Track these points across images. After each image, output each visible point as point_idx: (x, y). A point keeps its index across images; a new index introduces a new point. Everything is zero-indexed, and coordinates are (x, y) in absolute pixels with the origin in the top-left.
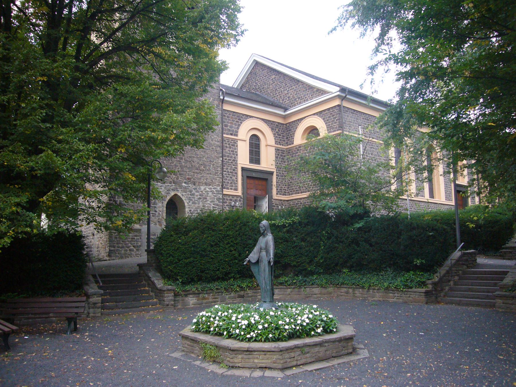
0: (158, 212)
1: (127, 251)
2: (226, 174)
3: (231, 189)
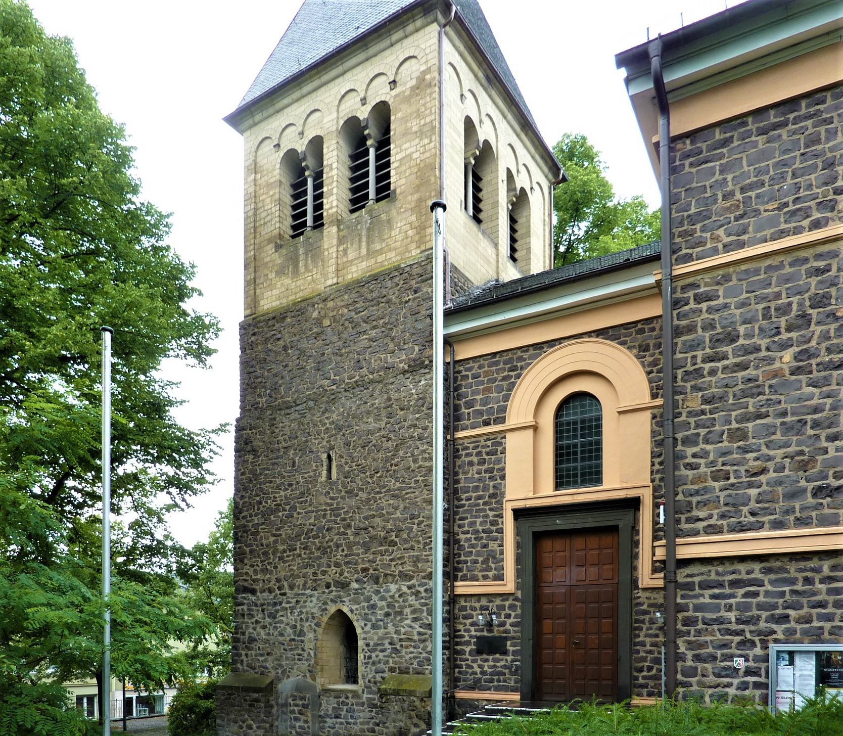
0: (308, 650)
2: (469, 540)
3: (485, 578)
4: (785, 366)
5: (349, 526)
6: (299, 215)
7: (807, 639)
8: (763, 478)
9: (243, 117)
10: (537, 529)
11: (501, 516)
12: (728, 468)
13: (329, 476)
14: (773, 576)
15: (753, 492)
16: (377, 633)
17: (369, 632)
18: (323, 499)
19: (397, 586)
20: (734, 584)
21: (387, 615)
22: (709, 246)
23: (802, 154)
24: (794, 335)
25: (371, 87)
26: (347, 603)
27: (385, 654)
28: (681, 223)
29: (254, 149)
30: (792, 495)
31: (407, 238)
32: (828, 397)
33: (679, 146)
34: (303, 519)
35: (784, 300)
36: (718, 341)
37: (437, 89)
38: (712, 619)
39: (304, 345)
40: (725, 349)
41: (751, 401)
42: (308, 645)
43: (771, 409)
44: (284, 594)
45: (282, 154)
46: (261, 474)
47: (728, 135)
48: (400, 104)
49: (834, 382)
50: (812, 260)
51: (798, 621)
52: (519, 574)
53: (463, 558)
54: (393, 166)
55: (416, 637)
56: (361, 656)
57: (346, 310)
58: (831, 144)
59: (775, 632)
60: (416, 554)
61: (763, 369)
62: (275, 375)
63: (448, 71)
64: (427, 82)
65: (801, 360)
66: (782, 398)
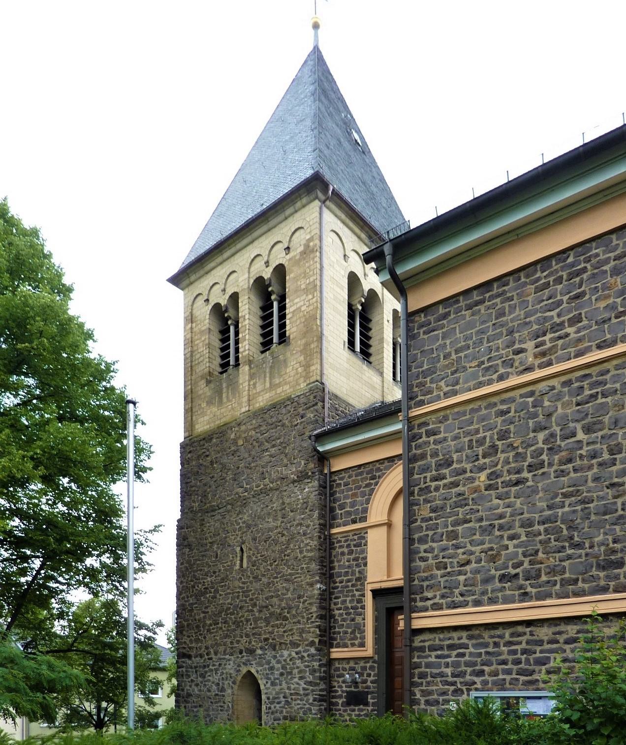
2: (341, 615)
3: (353, 645)
4: (481, 484)
5: (255, 605)
6: (225, 357)
7: (495, 688)
8: (468, 568)
9: (178, 280)
10: (388, 606)
11: (363, 595)
12: (446, 560)
13: (241, 566)
14: (474, 641)
15: (462, 578)
16: (274, 689)
17: (269, 688)
18: (237, 583)
19: (288, 652)
20: (451, 647)
21: (282, 674)
22: (435, 394)
23: (494, 324)
24: (487, 460)
25: (272, 252)
26: (254, 666)
27: (281, 705)
28: (418, 377)
29: (190, 303)
30: (487, 580)
31: (297, 374)
32: (509, 507)
33: (417, 319)
34: (224, 600)
35: (481, 435)
36: (440, 465)
37: (318, 254)
38: (436, 674)
39: (225, 460)
40: (444, 471)
41: (461, 510)
42: (228, 699)
43: (473, 516)
44: (211, 659)
45: (210, 307)
46: (194, 564)
47: (447, 310)
48: (293, 266)
49: (512, 495)
50: (499, 404)
51: (490, 675)
52: (376, 641)
53: (337, 630)
54: (288, 317)
55: (302, 692)
56: (264, 707)
57: (254, 433)
58: (512, 316)
59: (475, 683)
60: (301, 626)
61: (468, 486)
62: (205, 485)
63: (329, 239)
64: (311, 248)
65: (491, 480)
66: (480, 507)
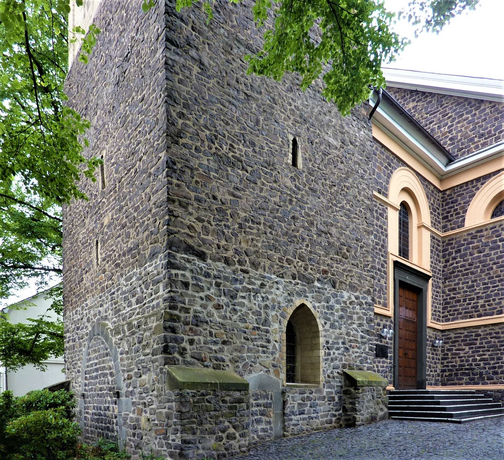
1: (220, 439)
